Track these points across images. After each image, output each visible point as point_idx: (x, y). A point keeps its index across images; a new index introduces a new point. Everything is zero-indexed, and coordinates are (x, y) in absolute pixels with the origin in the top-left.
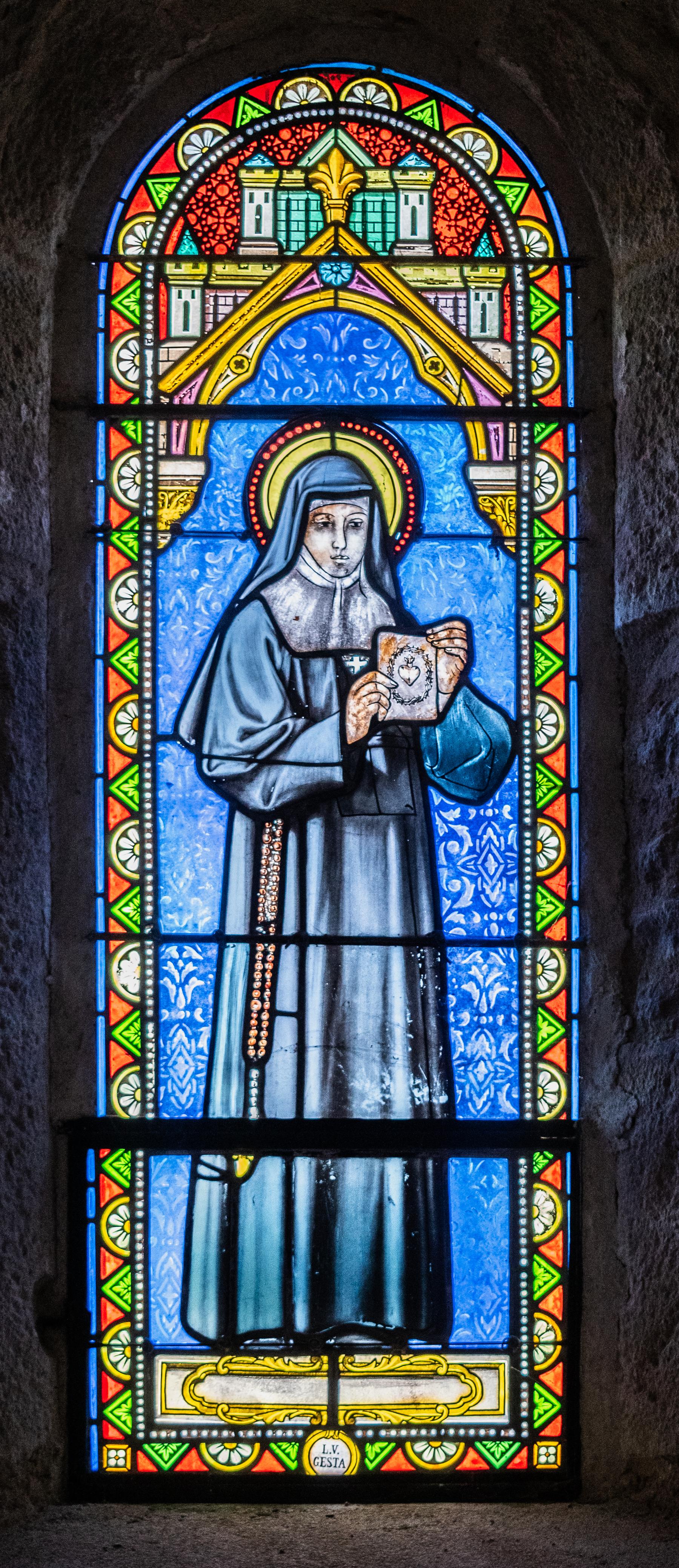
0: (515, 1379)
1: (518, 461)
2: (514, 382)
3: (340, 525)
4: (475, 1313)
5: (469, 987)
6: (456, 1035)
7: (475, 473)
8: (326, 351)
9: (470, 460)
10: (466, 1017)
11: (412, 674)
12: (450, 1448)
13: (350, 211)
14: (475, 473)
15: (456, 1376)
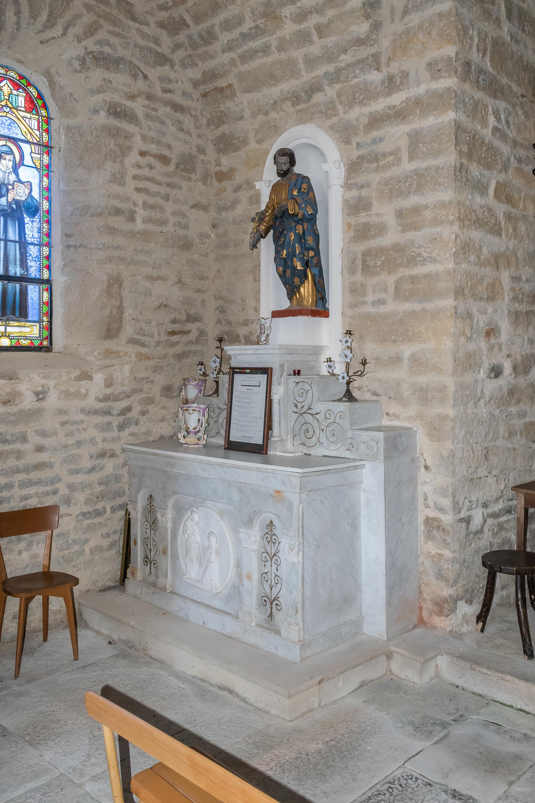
0: (40, 328)
1: (40, 154)
2: (40, 139)
3: (7, 160)
4: (33, 315)
5: (31, 252)
6: (29, 261)
7: (32, 155)
8: (5, 125)
9: (32, 152)
10: (30, 258)
11: (21, 191)
12: (28, 341)
13: (9, 97)
14: (32, 155)
15: (29, 327)
